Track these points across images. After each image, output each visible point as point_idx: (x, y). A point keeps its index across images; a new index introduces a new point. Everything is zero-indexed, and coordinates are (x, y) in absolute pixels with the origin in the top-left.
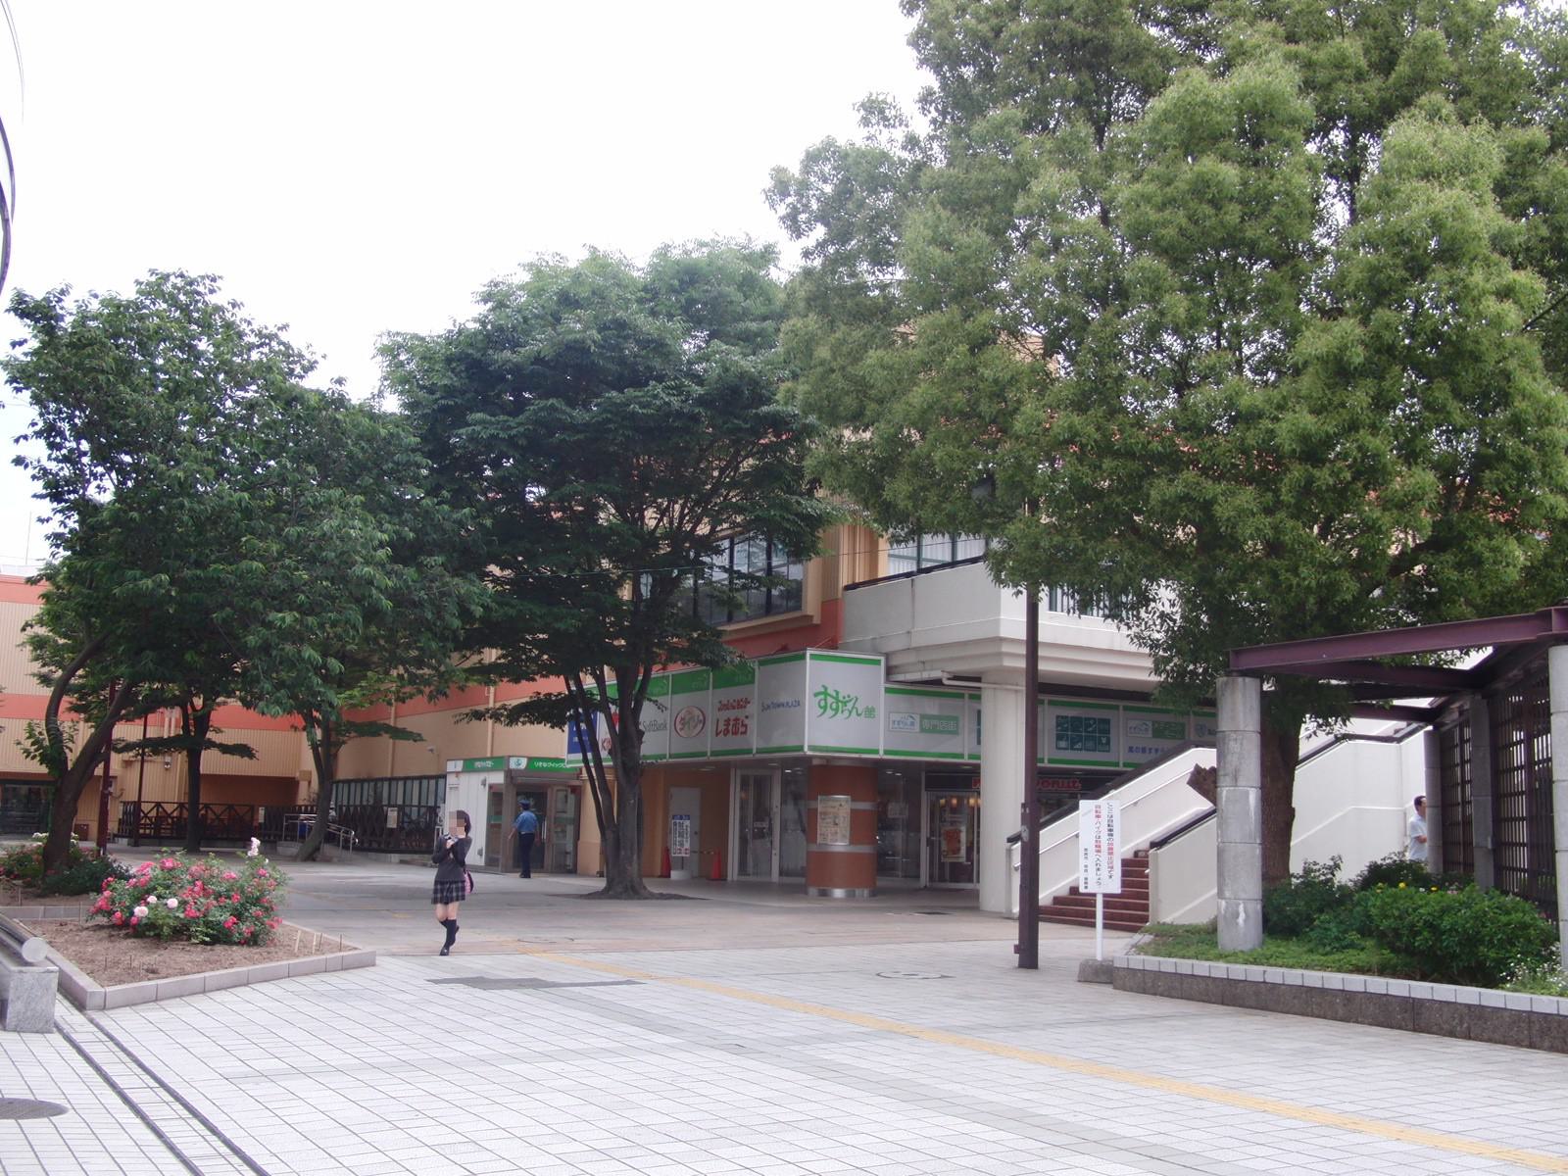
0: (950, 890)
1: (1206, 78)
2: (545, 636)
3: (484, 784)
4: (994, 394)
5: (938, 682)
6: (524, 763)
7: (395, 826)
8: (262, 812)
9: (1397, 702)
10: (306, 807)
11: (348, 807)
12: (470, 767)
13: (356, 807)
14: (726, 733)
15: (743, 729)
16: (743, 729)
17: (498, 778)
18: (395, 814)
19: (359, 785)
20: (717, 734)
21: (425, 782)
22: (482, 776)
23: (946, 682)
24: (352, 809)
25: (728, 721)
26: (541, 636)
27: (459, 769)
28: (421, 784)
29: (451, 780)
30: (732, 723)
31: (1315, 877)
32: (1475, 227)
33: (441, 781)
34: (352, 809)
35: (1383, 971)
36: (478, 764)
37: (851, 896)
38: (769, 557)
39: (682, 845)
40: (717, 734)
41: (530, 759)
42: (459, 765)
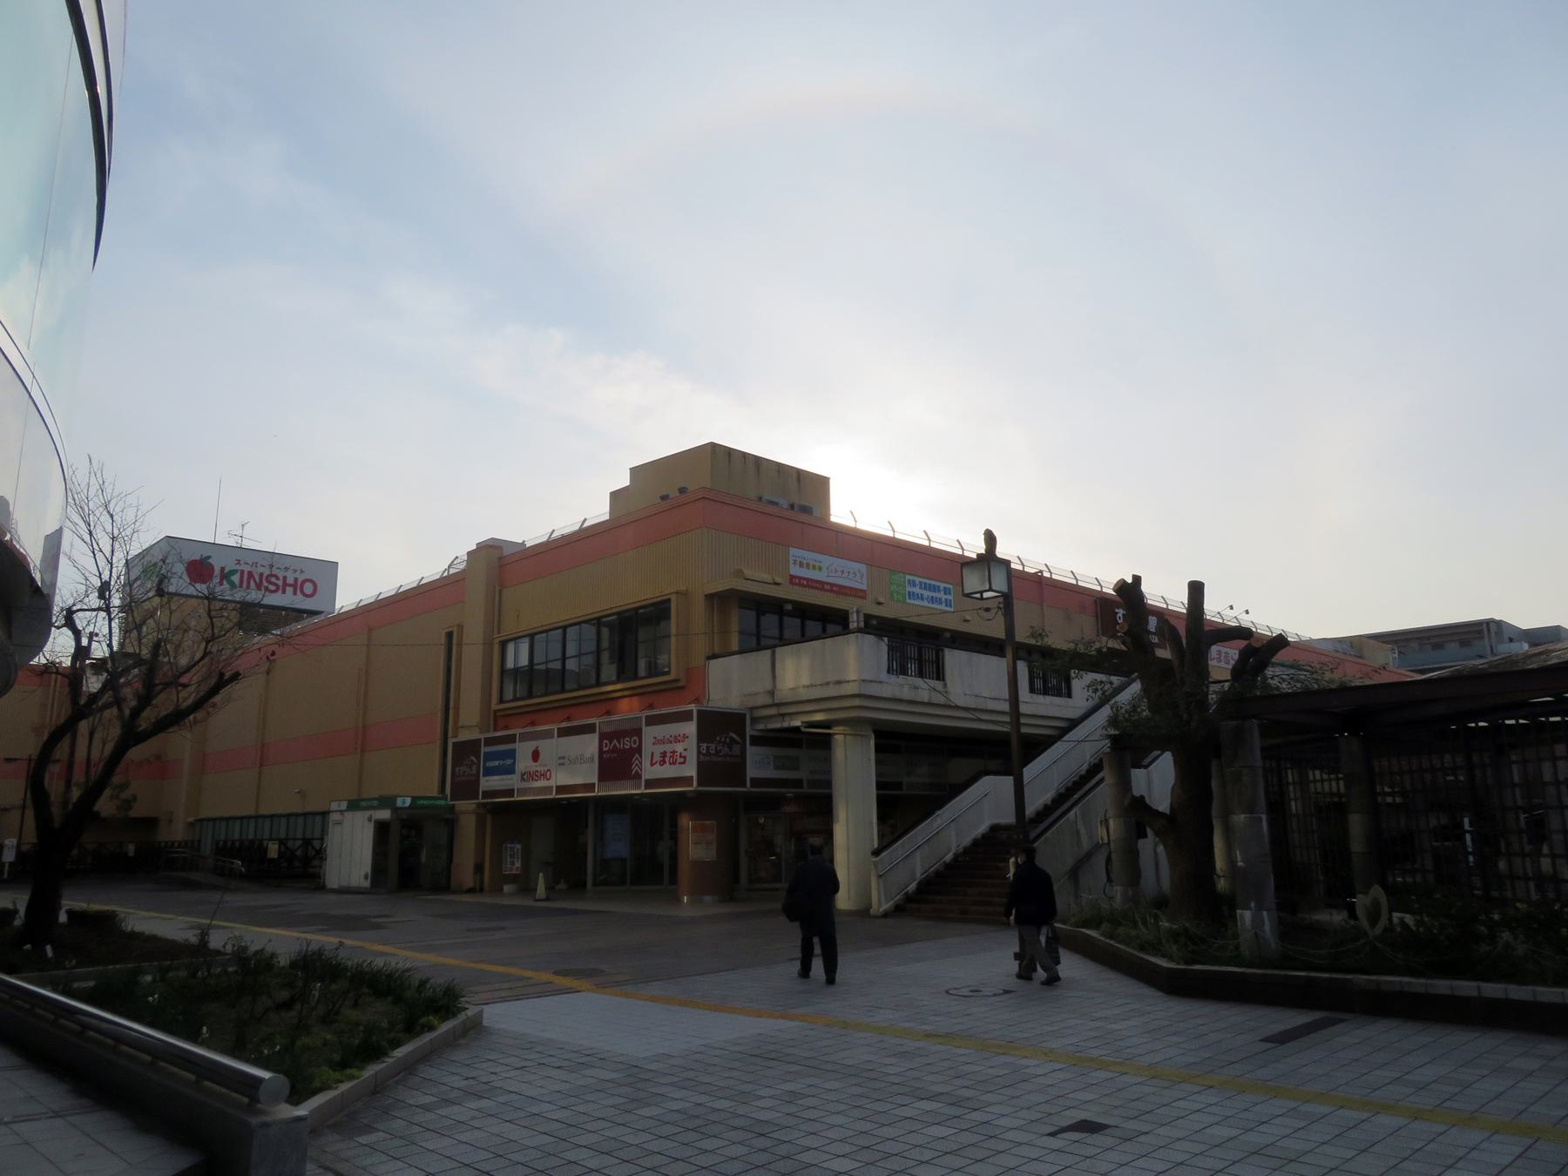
2: (1507, 722)
3: (370, 820)
4: (163, 579)
6: (408, 801)
7: (276, 856)
9: (816, 940)
12: (354, 805)
13: (233, 842)
14: (663, 762)
15: (682, 760)
16: (682, 760)
17: (385, 814)
18: (277, 846)
20: (652, 765)
22: (368, 813)
23: (803, 729)
25: (664, 754)
26: (1543, 719)
28: (272, 821)
29: (334, 817)
30: (668, 755)
35: (1267, 793)
36: (363, 804)
38: (53, 673)
39: (513, 864)
40: (652, 765)
41: (414, 799)
42: (344, 805)
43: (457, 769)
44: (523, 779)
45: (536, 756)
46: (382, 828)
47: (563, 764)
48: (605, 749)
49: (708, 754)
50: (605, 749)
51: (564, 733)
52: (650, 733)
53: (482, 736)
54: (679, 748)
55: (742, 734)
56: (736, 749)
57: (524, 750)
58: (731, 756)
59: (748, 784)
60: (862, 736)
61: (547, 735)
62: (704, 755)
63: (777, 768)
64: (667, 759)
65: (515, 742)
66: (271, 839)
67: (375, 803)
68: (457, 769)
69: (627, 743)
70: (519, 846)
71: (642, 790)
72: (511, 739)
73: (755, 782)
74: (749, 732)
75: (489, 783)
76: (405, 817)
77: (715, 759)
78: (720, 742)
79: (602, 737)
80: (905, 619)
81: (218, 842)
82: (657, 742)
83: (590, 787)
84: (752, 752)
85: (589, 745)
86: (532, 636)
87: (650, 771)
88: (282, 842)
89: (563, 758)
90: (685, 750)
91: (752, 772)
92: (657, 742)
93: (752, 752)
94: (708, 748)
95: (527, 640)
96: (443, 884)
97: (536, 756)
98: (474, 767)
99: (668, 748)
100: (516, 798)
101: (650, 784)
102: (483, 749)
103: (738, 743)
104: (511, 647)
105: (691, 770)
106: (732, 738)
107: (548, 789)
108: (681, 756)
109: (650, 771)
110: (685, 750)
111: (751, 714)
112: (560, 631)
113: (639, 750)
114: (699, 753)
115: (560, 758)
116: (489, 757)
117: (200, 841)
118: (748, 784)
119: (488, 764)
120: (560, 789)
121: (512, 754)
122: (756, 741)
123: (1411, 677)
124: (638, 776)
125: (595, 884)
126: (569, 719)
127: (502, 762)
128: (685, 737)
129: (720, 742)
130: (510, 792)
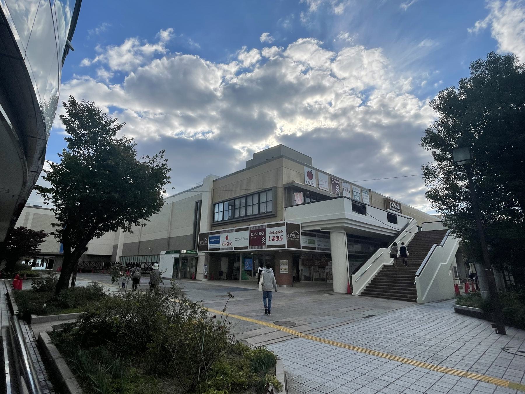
0: (286, 195)
1: (308, 128)
5: (319, 230)
8: (104, 263)
10: (118, 262)
11: (129, 263)
12: (168, 253)
13: (131, 262)
15: (281, 239)
17: (177, 256)
19: (125, 257)
20: (269, 241)
21: (143, 257)
24: (130, 263)
27: (165, 253)
29: (161, 256)
30: (276, 237)
31: (46, 108)
32: (406, 120)
33: (159, 256)
34: (130, 263)
37: (287, 287)
40: (269, 241)
42: (165, 252)
43: (200, 242)
44: (222, 245)
45: (227, 238)
46: (176, 261)
47: (237, 240)
48: (252, 236)
49: (289, 237)
50: (252, 236)
51: (237, 230)
52: (268, 230)
53: (209, 232)
54: (280, 235)
55: (299, 232)
56: (298, 236)
57: (223, 236)
58: (296, 238)
59: (301, 248)
60: (342, 233)
61: (231, 231)
62: (288, 237)
63: (309, 243)
64: (275, 239)
65: (125, 245)
66: (142, 262)
67: (173, 252)
68: (200, 242)
69: (260, 234)
70: (207, 267)
71: (266, 249)
72: (219, 232)
73: (303, 247)
74: (301, 231)
75: (210, 246)
76: (184, 256)
77: (292, 239)
78: (293, 233)
79: (251, 232)
80: (301, 187)
81: (127, 262)
82: (271, 233)
83: (247, 248)
84: (302, 237)
85: (246, 234)
86: (224, 202)
87: (268, 243)
88: (146, 263)
89: (237, 238)
90: (282, 236)
91: (302, 244)
92: (271, 233)
93: (302, 237)
94: (289, 235)
95: (222, 204)
96: (331, 253)
97: (227, 238)
98: (206, 242)
99: (276, 235)
100: (220, 251)
101: (268, 247)
102: (209, 236)
103: (298, 234)
104: (217, 206)
105: (285, 242)
106: (296, 232)
107: (231, 248)
108: (280, 238)
109: (268, 243)
110: (282, 236)
111: (301, 225)
112: (233, 201)
113: (265, 236)
114: (287, 237)
115: (235, 239)
116: (211, 238)
117: (122, 262)
118: (301, 248)
119: (211, 240)
120: (235, 248)
121: (219, 237)
122: (303, 234)
123: (63, 27)
124: (264, 244)
125: (242, 279)
126: (223, 229)
127: (215, 240)
128: (282, 231)
129: (293, 233)
130: (218, 249)
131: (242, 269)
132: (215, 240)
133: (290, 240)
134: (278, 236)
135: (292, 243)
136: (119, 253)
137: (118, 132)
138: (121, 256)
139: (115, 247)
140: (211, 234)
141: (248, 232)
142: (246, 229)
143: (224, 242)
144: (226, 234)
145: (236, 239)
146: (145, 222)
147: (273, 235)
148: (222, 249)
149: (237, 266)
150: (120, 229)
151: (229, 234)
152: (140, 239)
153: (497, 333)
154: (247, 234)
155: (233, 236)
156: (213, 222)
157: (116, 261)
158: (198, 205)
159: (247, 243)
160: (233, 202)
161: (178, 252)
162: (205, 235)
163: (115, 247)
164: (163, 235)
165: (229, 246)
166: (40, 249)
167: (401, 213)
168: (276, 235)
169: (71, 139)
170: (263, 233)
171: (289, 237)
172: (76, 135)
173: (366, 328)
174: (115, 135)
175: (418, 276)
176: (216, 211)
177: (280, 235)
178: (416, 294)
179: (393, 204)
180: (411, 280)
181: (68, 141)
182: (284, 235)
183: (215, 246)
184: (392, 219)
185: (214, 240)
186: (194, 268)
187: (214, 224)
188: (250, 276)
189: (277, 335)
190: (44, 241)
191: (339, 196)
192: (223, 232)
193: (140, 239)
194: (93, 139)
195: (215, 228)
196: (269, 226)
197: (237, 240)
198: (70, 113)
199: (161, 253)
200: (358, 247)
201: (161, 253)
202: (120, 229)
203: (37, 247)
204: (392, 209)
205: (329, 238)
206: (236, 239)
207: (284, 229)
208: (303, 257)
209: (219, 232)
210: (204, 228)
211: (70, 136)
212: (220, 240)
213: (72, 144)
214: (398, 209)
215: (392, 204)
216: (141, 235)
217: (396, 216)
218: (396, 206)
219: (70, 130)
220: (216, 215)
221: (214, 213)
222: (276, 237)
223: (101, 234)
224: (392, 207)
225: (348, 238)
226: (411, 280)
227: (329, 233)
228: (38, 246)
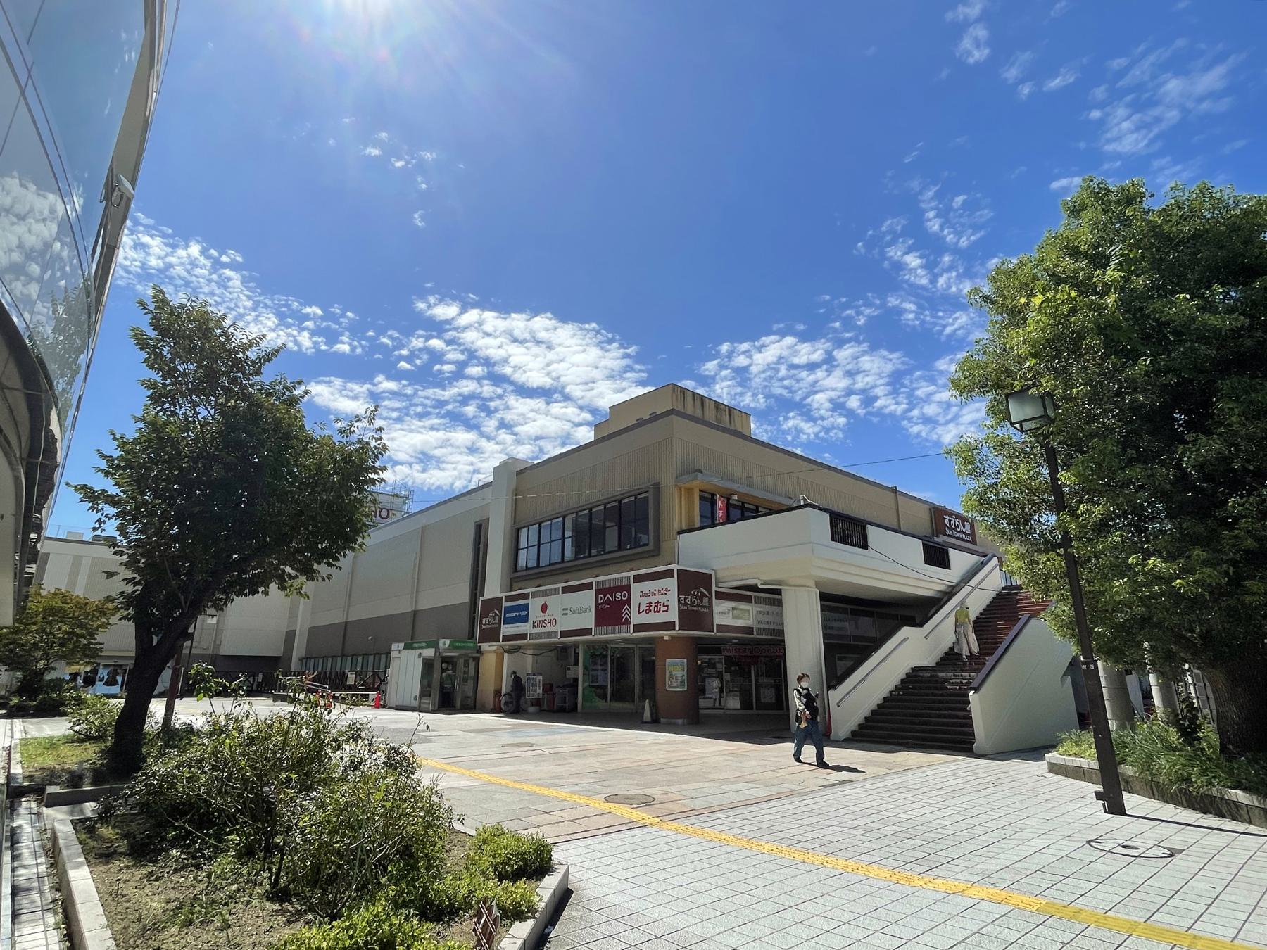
8: (261, 676)
15: (665, 609)
17: (430, 653)
20: (639, 613)
29: (394, 654)
30: (653, 605)
40: (639, 613)
42: (402, 645)
45: (544, 608)
46: (428, 665)
47: (567, 614)
49: (686, 604)
51: (566, 590)
52: (636, 588)
56: (706, 601)
57: (535, 605)
58: (702, 607)
61: (555, 592)
64: (652, 608)
72: (526, 596)
74: (714, 588)
75: (506, 630)
79: (598, 593)
82: (644, 595)
83: (587, 632)
87: (636, 619)
92: (644, 595)
97: (544, 608)
101: (638, 628)
102: (504, 604)
103: (706, 596)
104: (524, 533)
105: (673, 616)
106: (701, 592)
108: (664, 606)
109: (636, 619)
113: (628, 602)
116: (508, 610)
119: (508, 615)
120: (565, 634)
121: (526, 607)
124: (628, 622)
127: (518, 614)
131: (583, 684)
132: (518, 614)
133: (687, 610)
134: (658, 602)
135: (693, 617)
136: (298, 650)
137: (266, 369)
138: (303, 658)
139: (290, 636)
140: (508, 599)
141: (591, 594)
142: (588, 586)
143: (538, 619)
144: (541, 601)
145: (566, 612)
146: (332, 571)
147: (647, 600)
148: (533, 636)
149: (573, 676)
150: (273, 587)
151: (549, 600)
152: (347, 614)
153: (1105, 812)
154: (588, 598)
155: (558, 603)
156: (516, 570)
157: (292, 669)
158: (480, 531)
159: (588, 621)
160: (561, 524)
161: (434, 645)
162: (497, 602)
163: (290, 636)
164: (403, 606)
165: (549, 629)
166: (101, 642)
167: (974, 542)
168: (654, 599)
169: (156, 382)
170: (625, 596)
171: (686, 604)
172: (170, 372)
173: (814, 807)
174: (258, 373)
175: (976, 690)
176: (523, 544)
177: (662, 599)
178: (973, 734)
179: (952, 522)
180: (959, 702)
181: (149, 388)
182: (673, 599)
183: (516, 629)
184: (936, 556)
185: (514, 614)
186: (471, 683)
187: (516, 575)
188: (602, 699)
189: (604, 821)
190: (111, 625)
191: (802, 503)
192: (535, 595)
193: (347, 614)
194: (208, 384)
195: (520, 585)
196: (638, 579)
197: (567, 614)
198: (155, 323)
199: (394, 646)
200: (848, 626)
201: (394, 646)
202: (273, 587)
203: (95, 639)
204: (951, 533)
205: (779, 603)
206: (566, 612)
207: (672, 583)
208: (730, 653)
209: (526, 596)
210: (493, 588)
211: (155, 376)
212: (527, 615)
213: (158, 397)
214: (965, 533)
215: (950, 521)
216: (349, 606)
217: (947, 550)
218: (961, 526)
219: (155, 361)
220: (522, 554)
221: (517, 549)
222: (653, 605)
223: (226, 600)
224: (951, 528)
225: (823, 602)
226: (959, 702)
227: (779, 592)
228: (96, 636)
